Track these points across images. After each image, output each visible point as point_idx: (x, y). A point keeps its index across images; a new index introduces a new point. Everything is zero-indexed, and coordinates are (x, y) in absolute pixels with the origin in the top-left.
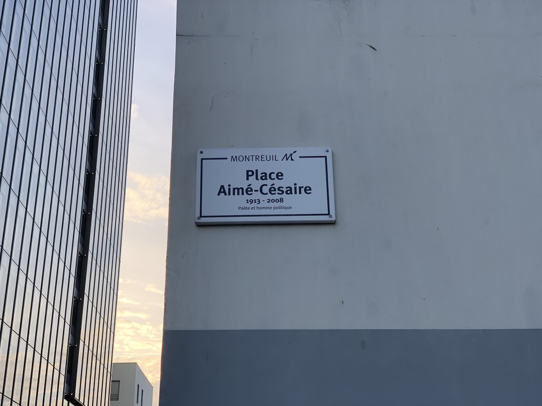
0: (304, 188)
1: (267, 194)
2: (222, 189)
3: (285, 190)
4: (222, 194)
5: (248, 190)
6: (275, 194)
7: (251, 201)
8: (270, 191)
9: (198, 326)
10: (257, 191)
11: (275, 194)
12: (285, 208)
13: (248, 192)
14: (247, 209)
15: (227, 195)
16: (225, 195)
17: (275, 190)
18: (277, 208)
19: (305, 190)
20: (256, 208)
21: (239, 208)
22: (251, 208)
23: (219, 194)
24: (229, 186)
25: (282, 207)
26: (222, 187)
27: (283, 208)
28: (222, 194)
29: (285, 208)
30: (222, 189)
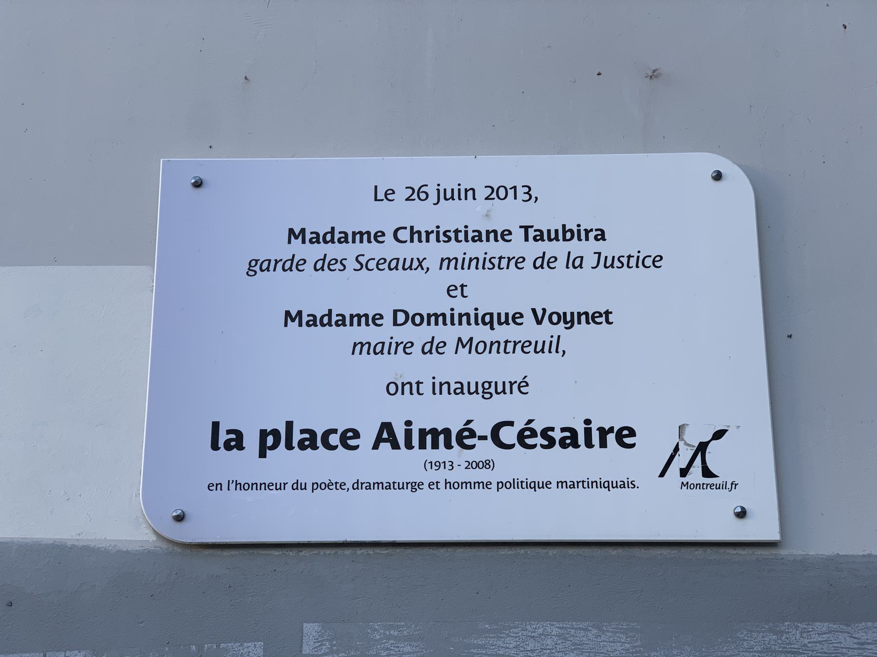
0: (339, 432)
3: (557, 435)
4: (385, 446)
5: (347, 435)
6: (534, 446)
7: (438, 464)
8: (521, 437)
10: (484, 438)
11: (534, 446)
12: (532, 485)
14: (338, 487)
15: (399, 448)
16: (393, 448)
19: (620, 440)
20: (442, 485)
21: (313, 489)
24: (408, 423)
25: (522, 482)
28: (385, 446)
29: (532, 485)
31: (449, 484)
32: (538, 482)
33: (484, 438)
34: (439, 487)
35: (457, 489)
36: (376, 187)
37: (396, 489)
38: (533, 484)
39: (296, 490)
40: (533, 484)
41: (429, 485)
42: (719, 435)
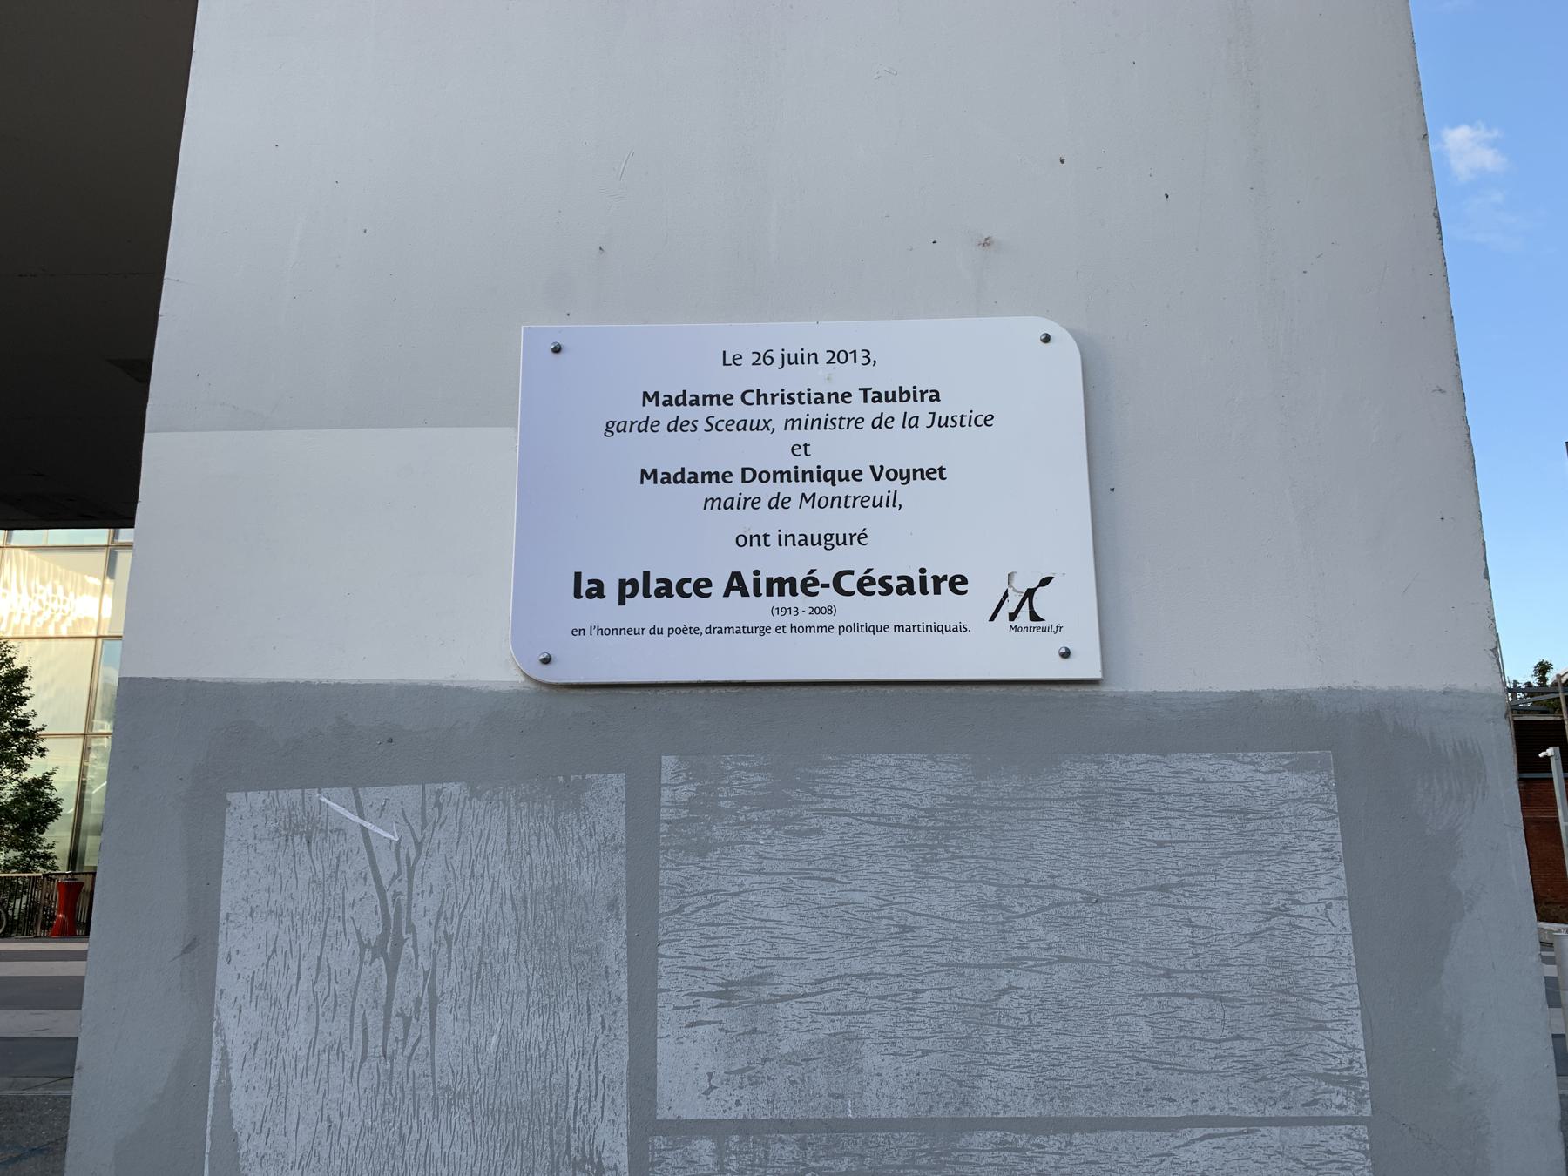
0: (693, 581)
1: (852, 594)
2: (735, 580)
4: (735, 594)
6: (873, 593)
8: (861, 585)
9: (68, 853)
10: (827, 586)
11: (873, 593)
13: (701, 590)
17: (872, 582)
18: (849, 629)
20: (788, 629)
21: (669, 634)
22: (836, 630)
23: (726, 594)
24: (757, 572)
25: (862, 626)
26: (736, 576)
27: (864, 629)
28: (735, 594)
30: (735, 580)
33: (827, 586)
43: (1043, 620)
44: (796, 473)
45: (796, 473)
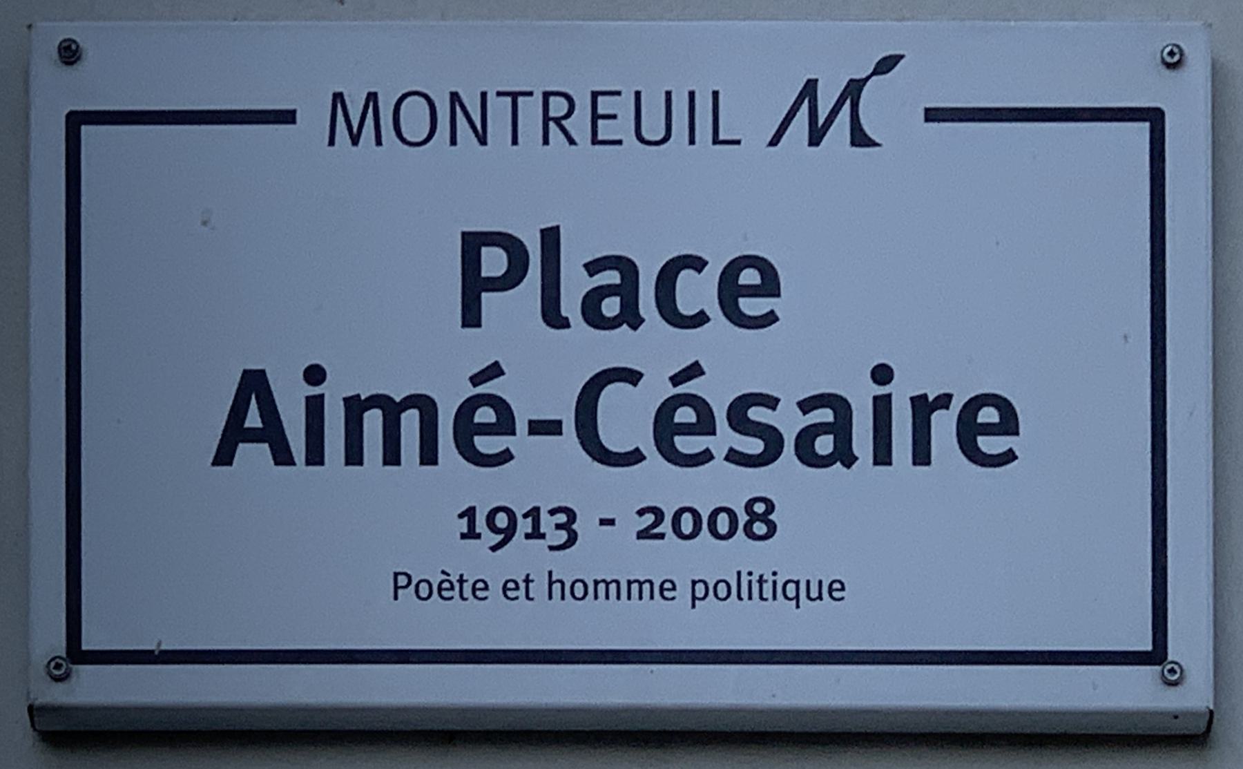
1: (635, 457)
4: (253, 455)
6: (705, 457)
7: (502, 520)
10: (552, 428)
11: (705, 457)
14: (467, 591)
15: (293, 463)
20: (539, 588)
22: (683, 591)
28: (253, 455)
31: (559, 585)
32: (808, 582)
33: (552, 428)
34: (531, 595)
35: (725, 599)
36: (932, 115)
37: (766, 600)
38: (791, 587)
39: (818, 601)
40: (791, 587)
41: (505, 589)
42: (887, 65)
43: (876, 144)
44: (882, 406)
45: (882, 406)
